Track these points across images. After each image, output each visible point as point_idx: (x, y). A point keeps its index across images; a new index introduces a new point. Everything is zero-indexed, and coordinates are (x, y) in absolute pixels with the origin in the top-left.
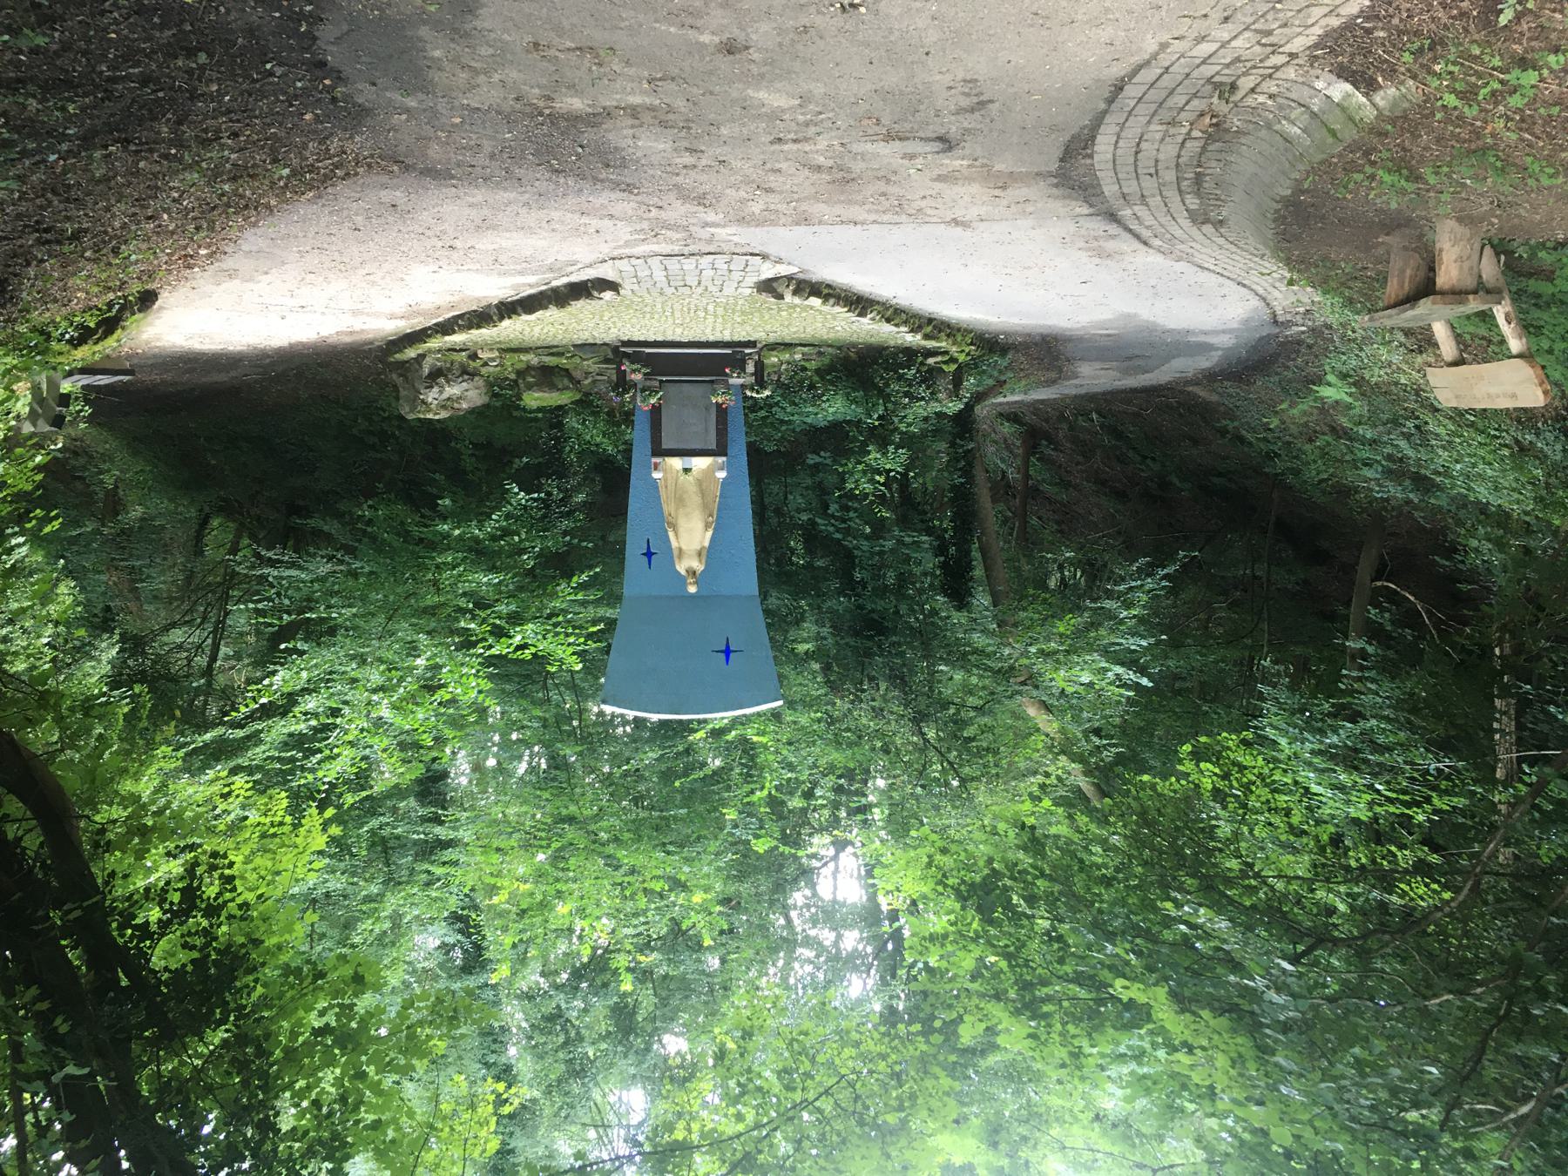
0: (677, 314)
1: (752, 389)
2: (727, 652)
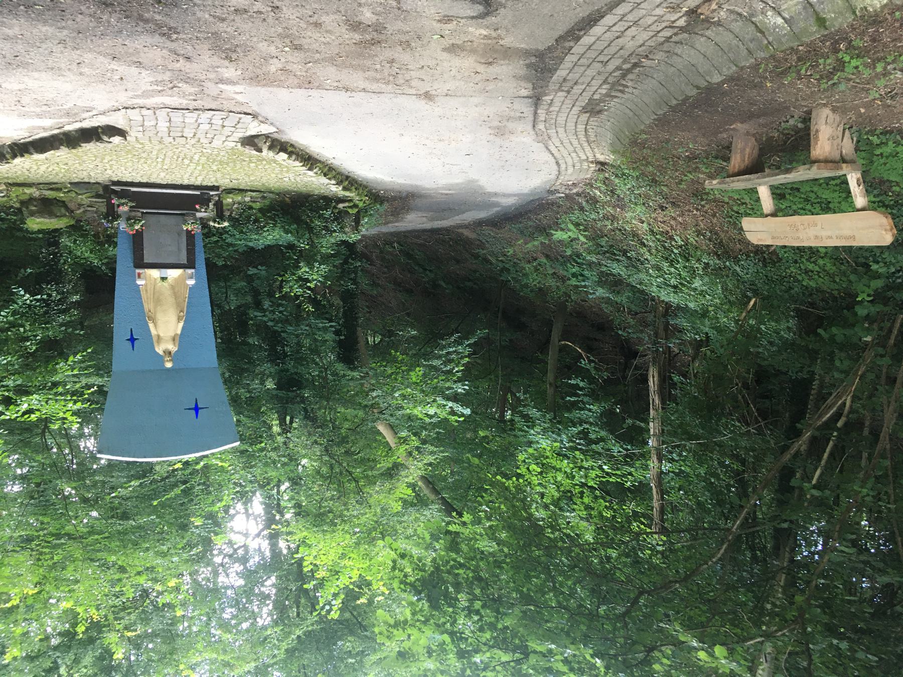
0: (167, 161)
1: (215, 221)
2: (197, 409)
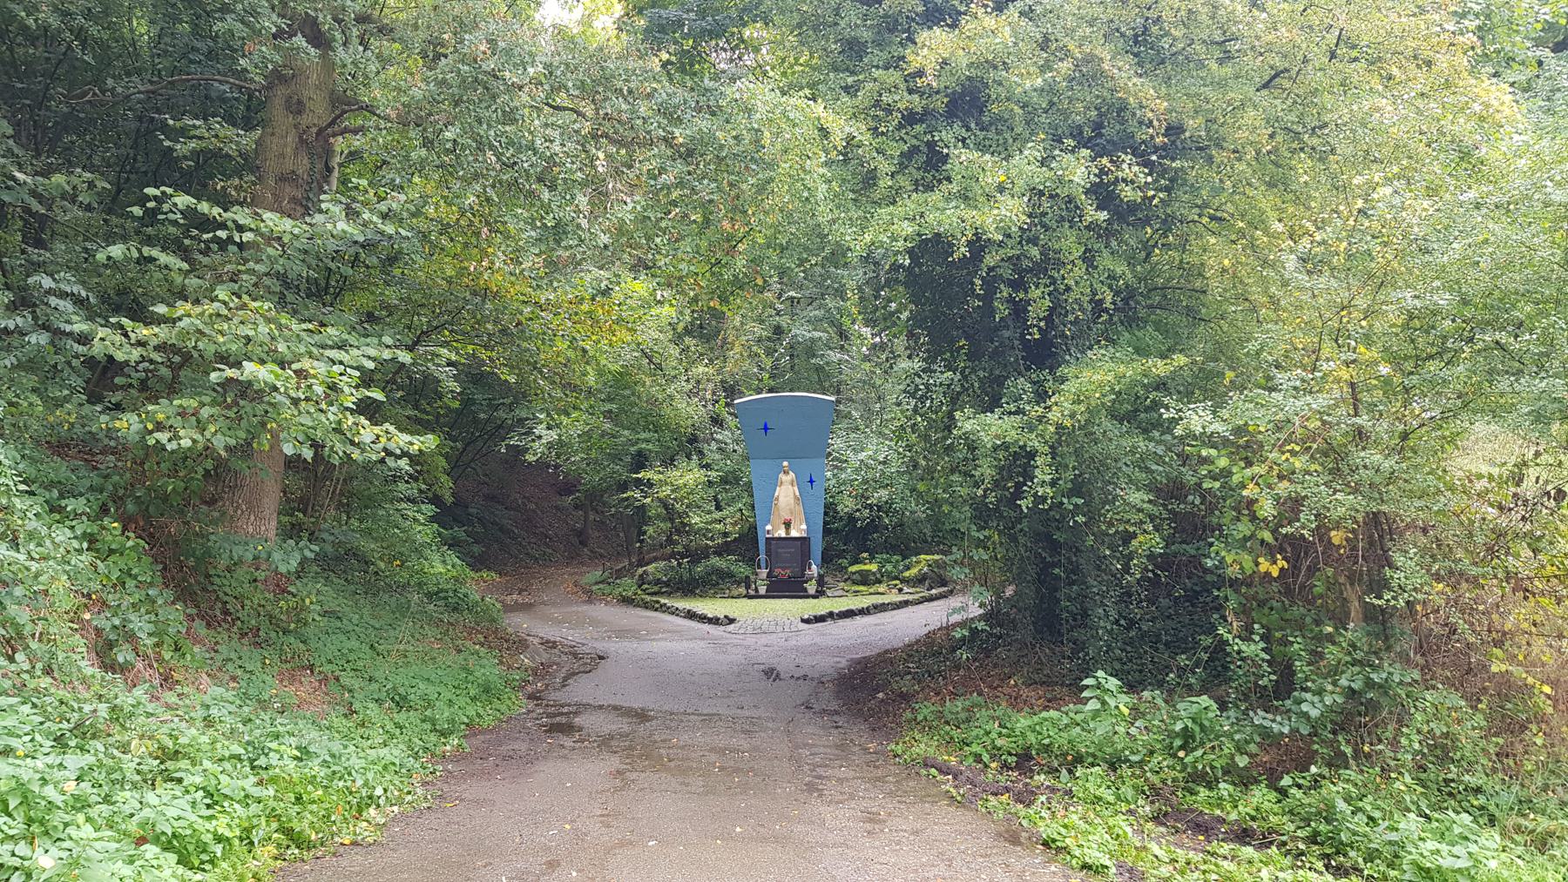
2: (766, 429)
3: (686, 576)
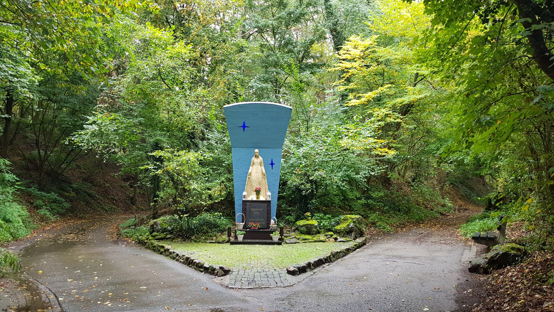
2: (244, 127)
3: (185, 226)
